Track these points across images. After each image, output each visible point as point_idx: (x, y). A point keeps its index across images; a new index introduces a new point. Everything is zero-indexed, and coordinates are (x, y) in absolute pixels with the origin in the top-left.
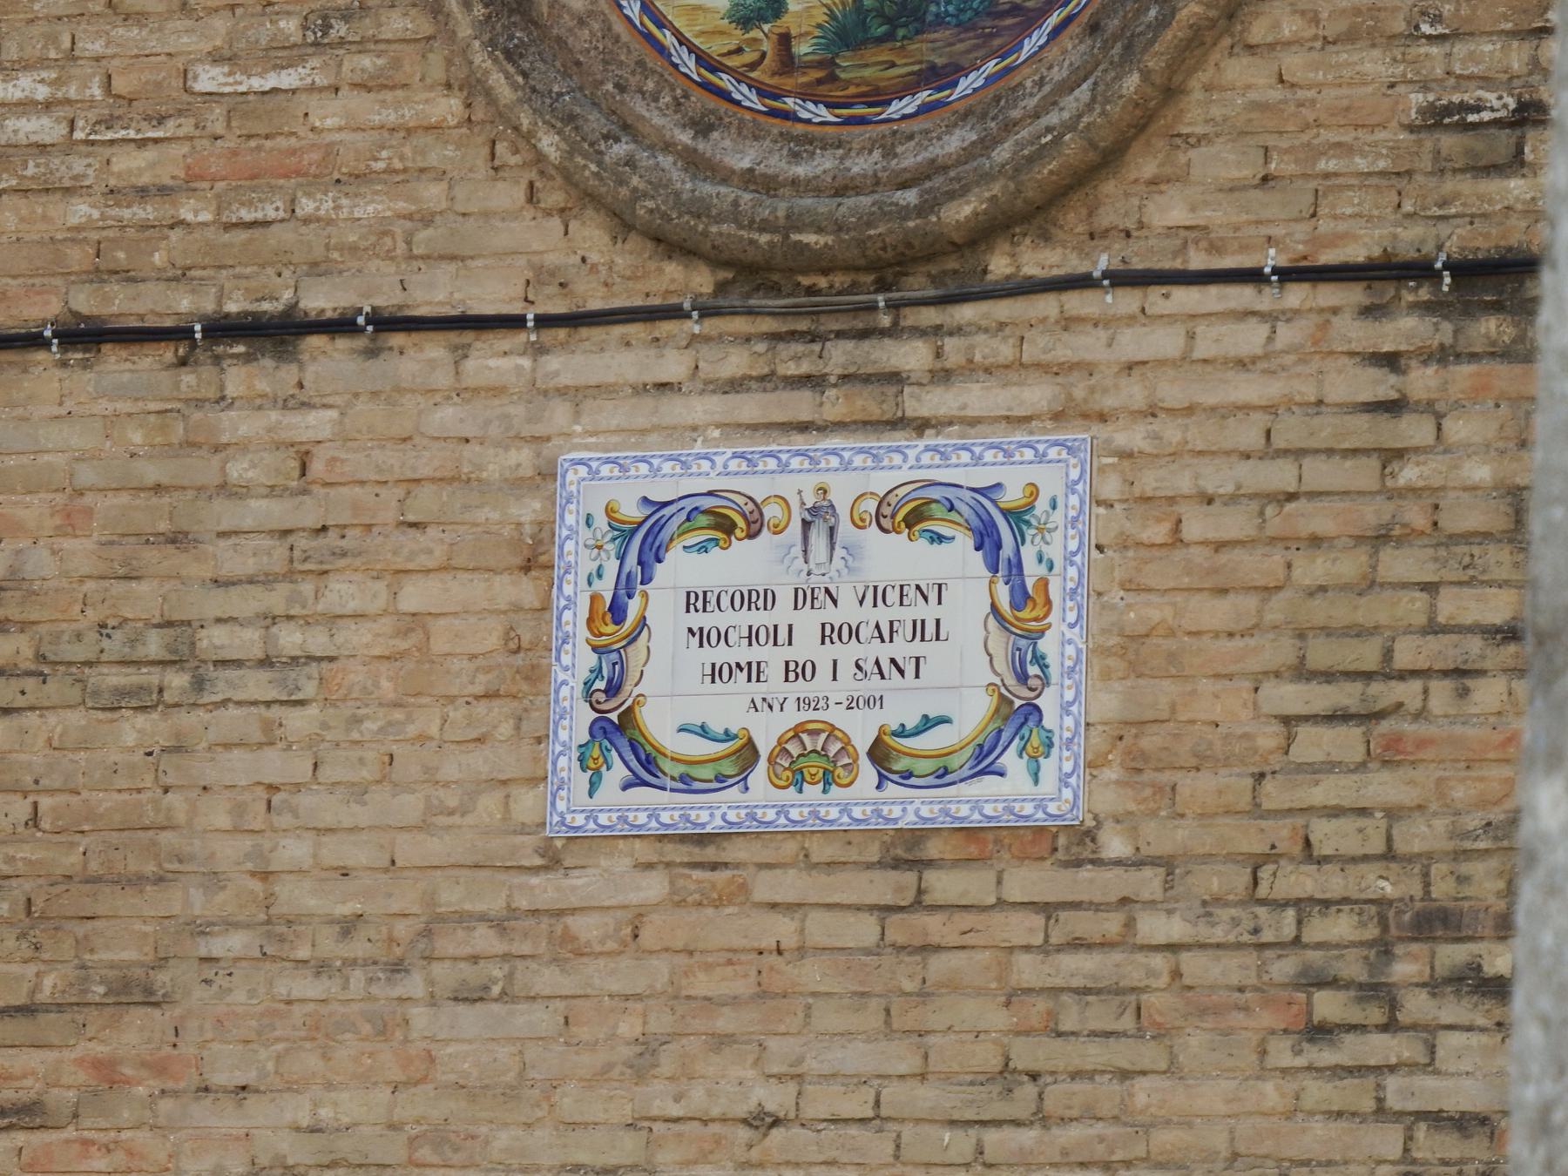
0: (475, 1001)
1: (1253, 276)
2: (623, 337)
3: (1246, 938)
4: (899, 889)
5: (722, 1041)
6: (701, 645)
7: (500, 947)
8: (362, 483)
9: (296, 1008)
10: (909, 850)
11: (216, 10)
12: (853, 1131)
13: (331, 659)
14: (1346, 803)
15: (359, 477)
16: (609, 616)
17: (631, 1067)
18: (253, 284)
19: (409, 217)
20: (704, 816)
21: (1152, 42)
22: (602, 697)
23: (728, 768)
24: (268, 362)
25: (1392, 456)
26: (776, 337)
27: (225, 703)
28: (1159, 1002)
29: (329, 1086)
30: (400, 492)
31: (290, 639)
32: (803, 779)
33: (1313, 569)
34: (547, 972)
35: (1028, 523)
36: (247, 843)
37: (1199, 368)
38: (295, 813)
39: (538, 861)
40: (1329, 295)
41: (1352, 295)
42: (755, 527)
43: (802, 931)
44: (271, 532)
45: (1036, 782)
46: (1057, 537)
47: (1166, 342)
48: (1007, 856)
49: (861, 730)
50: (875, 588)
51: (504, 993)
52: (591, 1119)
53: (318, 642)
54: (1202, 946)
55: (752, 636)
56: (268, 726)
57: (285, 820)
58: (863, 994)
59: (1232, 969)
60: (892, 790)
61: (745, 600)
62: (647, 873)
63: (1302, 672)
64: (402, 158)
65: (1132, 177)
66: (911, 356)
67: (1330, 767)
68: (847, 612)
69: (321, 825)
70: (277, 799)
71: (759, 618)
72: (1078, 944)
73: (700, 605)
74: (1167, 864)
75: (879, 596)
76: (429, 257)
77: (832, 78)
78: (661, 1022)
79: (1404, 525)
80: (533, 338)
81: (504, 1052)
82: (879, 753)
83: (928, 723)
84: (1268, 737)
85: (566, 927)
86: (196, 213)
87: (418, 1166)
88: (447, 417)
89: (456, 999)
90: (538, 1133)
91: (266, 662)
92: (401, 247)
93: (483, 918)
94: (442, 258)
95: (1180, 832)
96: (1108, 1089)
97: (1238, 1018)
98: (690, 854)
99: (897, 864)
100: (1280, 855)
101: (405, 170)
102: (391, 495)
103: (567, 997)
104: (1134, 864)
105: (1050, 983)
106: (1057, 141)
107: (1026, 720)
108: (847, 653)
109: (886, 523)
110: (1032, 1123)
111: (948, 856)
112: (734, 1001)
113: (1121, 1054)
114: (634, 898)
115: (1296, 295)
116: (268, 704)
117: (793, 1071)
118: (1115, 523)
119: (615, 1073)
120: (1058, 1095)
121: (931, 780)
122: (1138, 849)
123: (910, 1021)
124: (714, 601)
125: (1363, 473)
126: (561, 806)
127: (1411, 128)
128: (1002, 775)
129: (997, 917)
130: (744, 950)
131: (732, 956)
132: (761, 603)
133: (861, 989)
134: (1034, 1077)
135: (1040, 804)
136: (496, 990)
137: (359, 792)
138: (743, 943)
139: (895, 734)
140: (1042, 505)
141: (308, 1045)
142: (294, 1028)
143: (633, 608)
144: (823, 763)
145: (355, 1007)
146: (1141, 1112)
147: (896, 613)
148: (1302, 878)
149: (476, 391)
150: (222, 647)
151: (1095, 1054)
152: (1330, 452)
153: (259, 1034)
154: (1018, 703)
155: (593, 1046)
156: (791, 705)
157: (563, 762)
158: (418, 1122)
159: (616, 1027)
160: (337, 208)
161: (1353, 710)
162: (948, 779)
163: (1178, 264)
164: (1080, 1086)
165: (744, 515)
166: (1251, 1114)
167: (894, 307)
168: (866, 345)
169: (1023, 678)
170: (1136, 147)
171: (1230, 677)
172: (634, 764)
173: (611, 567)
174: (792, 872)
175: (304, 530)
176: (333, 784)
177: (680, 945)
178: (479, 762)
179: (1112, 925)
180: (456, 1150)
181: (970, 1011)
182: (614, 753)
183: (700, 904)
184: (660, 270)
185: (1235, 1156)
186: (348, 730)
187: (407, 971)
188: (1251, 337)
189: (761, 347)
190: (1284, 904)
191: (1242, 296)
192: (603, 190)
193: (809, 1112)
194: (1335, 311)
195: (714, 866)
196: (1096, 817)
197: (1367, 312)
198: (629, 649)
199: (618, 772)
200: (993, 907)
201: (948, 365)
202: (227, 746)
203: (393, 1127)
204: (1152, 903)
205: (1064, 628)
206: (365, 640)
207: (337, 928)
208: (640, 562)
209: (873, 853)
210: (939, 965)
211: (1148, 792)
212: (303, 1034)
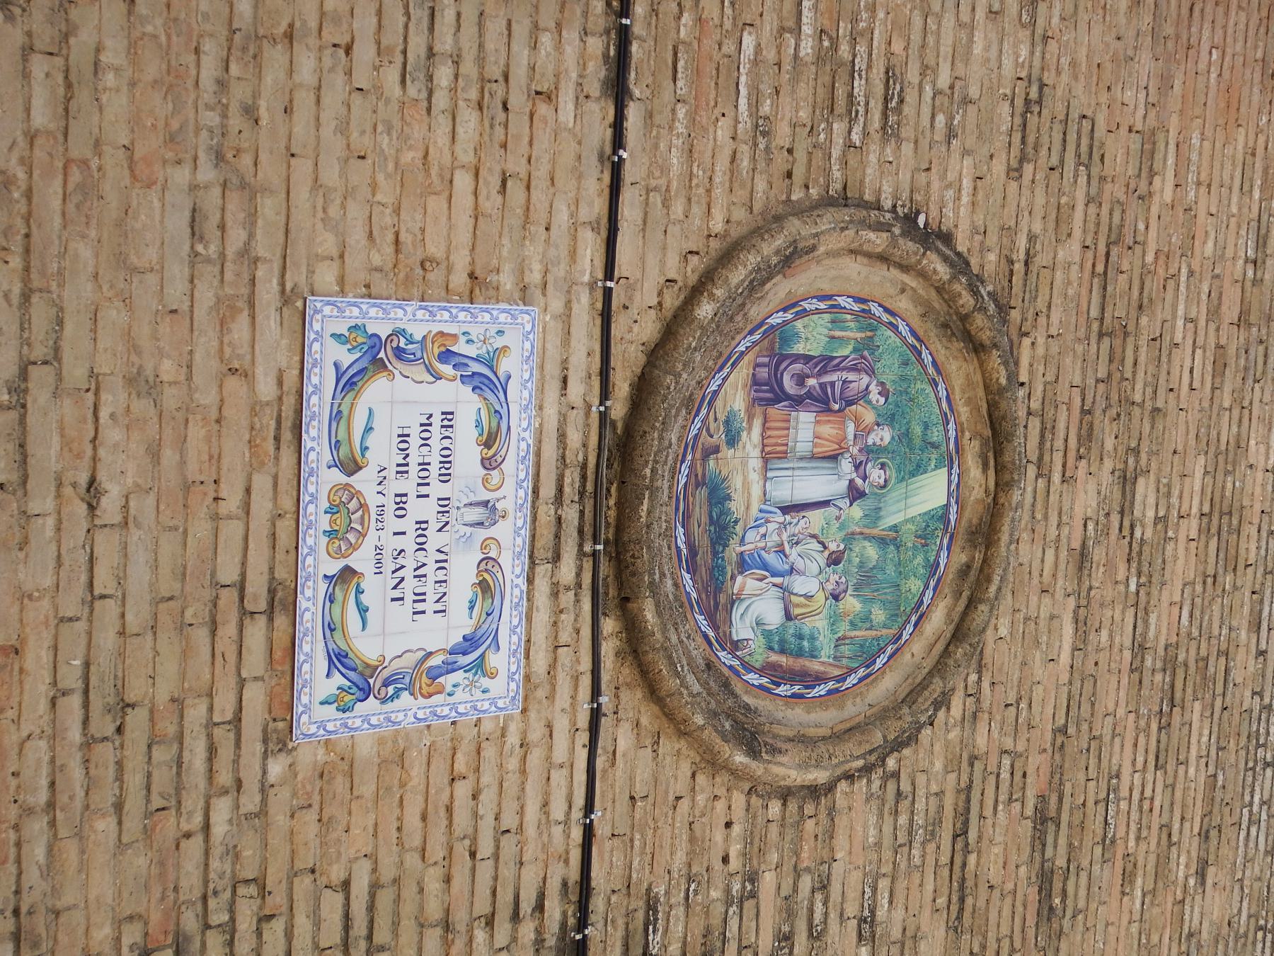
0: (192, 228)
1: (589, 807)
2: (593, 351)
3: (211, 886)
4: (256, 598)
5: (154, 454)
6: (422, 425)
7: (230, 252)
8: (531, 144)
9: (193, 57)
10: (281, 600)
11: (779, 53)
12: (84, 578)
13: (429, 110)
14: (295, 942)
15: (535, 142)
16: (443, 349)
17: (139, 373)
18: (645, 66)
19: (668, 190)
20: (313, 433)
21: (716, 731)
22: (394, 345)
23: (344, 450)
24: (603, 74)
25: (490, 922)
26: (584, 467)
27: (408, 15)
28: (169, 826)
29: (133, 84)
30: (524, 175)
31: (443, 75)
32: (333, 514)
33: (433, 885)
34: (210, 295)
35: (476, 673)
36: (313, 24)
37: (545, 775)
38: (331, 70)
39: (289, 286)
40: (575, 856)
41: (574, 874)
42: (487, 462)
43: (230, 517)
44: (508, 65)
45: (322, 703)
46: (467, 697)
47: (560, 754)
48: (273, 683)
49: (361, 560)
50: (446, 561)
51: (197, 254)
52: (99, 337)
53: (441, 100)
54: (207, 853)
55: (424, 466)
56: (390, 50)
57: (327, 62)
58: (184, 575)
59: (191, 883)
60: (323, 586)
61: (446, 461)
62: (275, 381)
63: (375, 887)
64: (697, 185)
65: (642, 710)
66: (567, 571)
67: (317, 924)
68: (435, 540)
69: (322, 93)
70: (341, 52)
71: (434, 469)
72: (212, 751)
73: (446, 423)
74: (263, 812)
75: (442, 565)
76: (647, 204)
77: (697, 485)
78: (171, 399)
79: (453, 941)
80: (600, 284)
81: (152, 254)
82: (348, 573)
83: (363, 610)
84: (336, 874)
85: (242, 310)
86: (685, 25)
87: (65, 168)
88: (562, 217)
89: (194, 210)
90: (89, 286)
91: (431, 54)
92: (653, 183)
93: (251, 236)
94: (646, 214)
95: (282, 818)
96: (105, 796)
97: (156, 892)
98: (287, 418)
99: (272, 592)
100: (264, 897)
101: (690, 187)
102: (522, 169)
103: (192, 312)
104: (263, 785)
105: (187, 732)
106: (677, 675)
107: (360, 689)
108: (409, 543)
109: (483, 566)
110: (85, 735)
111: (275, 633)
112: (183, 462)
113: (134, 804)
114: (259, 370)
115: (577, 834)
116: (404, 52)
117: (131, 520)
118: (469, 734)
119: (134, 358)
120: (105, 754)
121: (327, 618)
122: (272, 786)
123: (164, 619)
124: (447, 434)
125: (482, 907)
126: (327, 310)
127: (649, 890)
128: (328, 676)
129: (232, 681)
130: (219, 469)
131: (216, 459)
132: (443, 471)
133: (188, 572)
134: (119, 730)
135: (307, 708)
136: (200, 248)
137: (343, 128)
138: (224, 468)
139: (358, 585)
140: (485, 682)
141: (164, 67)
142: (178, 55)
143: (447, 369)
144: (343, 529)
145: (192, 115)
146: (91, 826)
147: (431, 578)
148: (248, 919)
149: (575, 238)
150: (443, 17)
151: (134, 781)
152: (496, 878)
153: (176, 20)
154: (371, 681)
155: (155, 337)
156: (380, 500)
157: (356, 311)
158: (100, 169)
159: (169, 357)
160: (678, 136)
161: (351, 933)
162: (328, 632)
163: (599, 751)
164: (111, 771)
165: (494, 455)
166: (88, 919)
167: (595, 554)
168: (575, 534)
169: (386, 684)
170: (656, 709)
171: (375, 835)
172: (351, 372)
173: (471, 351)
174: (270, 505)
175: (507, 93)
176: (349, 106)
177: (225, 413)
178: (357, 237)
179: (224, 777)
180: (77, 207)
181: (169, 667)
182: (359, 354)
183: (252, 428)
184: (625, 381)
185: (57, 914)
186: (384, 121)
187: (216, 166)
188: (558, 811)
189: (580, 458)
190: (232, 911)
191: (580, 800)
192: (681, 350)
193: (100, 537)
194: (567, 862)
195: (277, 439)
196: (294, 749)
197: (565, 884)
198: (422, 367)
199: (347, 359)
200: (239, 675)
201: (561, 595)
202: (379, 13)
203: (97, 143)
204: (237, 807)
205: (414, 710)
206: (439, 140)
207: (250, 102)
208: (474, 374)
209: (281, 573)
210: (201, 636)
211: (309, 788)
212: (173, 63)
